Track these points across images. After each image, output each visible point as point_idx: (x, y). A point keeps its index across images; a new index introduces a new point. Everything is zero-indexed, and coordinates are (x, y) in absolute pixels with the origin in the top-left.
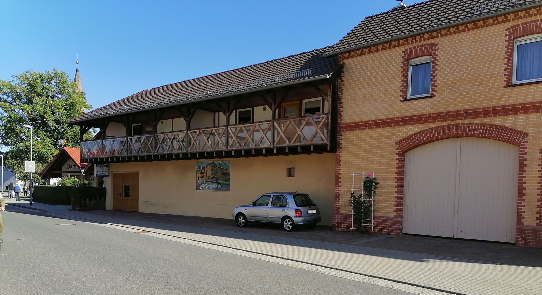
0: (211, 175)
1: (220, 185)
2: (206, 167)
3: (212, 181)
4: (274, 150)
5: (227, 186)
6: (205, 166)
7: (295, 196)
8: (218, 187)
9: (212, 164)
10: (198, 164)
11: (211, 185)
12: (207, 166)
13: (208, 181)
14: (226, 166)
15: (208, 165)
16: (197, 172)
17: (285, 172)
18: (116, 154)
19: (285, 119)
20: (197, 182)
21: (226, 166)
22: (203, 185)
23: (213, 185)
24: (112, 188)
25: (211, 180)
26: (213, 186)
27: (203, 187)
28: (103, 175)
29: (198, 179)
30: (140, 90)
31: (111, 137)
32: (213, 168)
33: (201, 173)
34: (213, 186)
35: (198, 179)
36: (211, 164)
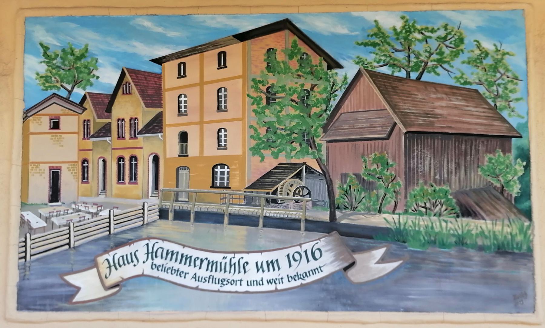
0: (255, 150)
1: (379, 253)
2: (171, 67)
4: (503, 154)
6: (159, 61)
8: (355, 275)
9: (269, 41)
11: (252, 258)
12: (192, 62)
13: (201, 217)
14: (476, 62)
15: (193, 51)
16: (27, 114)
17: (99, 79)
18: (484, 96)
19: (477, 213)
20: (23, 223)
21: (476, 62)
22: (126, 260)
23: (281, 256)
25: (249, 202)
26: (272, 264)
27: (128, 271)
28: (79, 108)
29: (55, 196)
32: (272, 79)
33: (105, 131)
34: (272, 264)
35: (55, 196)
36: (242, 37)
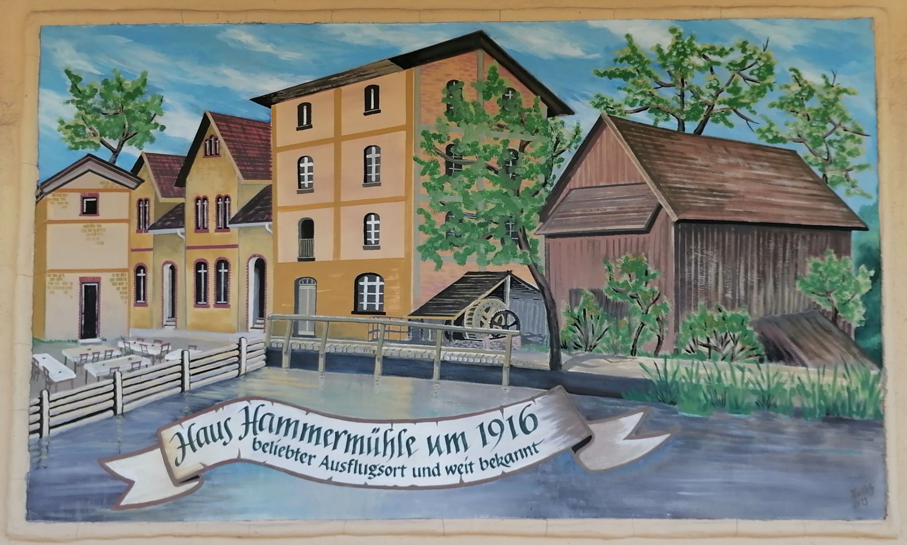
2: (286, 112)
3: (454, 353)
5: (811, 438)
6: (266, 101)
7: (380, 157)
8: (592, 459)
9: (451, 67)
10: (87, 49)
11: (421, 431)
12: (321, 102)
14: (793, 105)
15: (323, 84)
16: (42, 189)
20: (37, 373)
21: (793, 105)
23: (469, 426)
24: (640, 164)
25: (417, 336)
26: (454, 441)
27: (213, 453)
29: (89, 328)
30: (364, 92)
31: (739, 240)
32: (455, 132)
33: (175, 217)
35: (89, 328)
36: (406, 61)
